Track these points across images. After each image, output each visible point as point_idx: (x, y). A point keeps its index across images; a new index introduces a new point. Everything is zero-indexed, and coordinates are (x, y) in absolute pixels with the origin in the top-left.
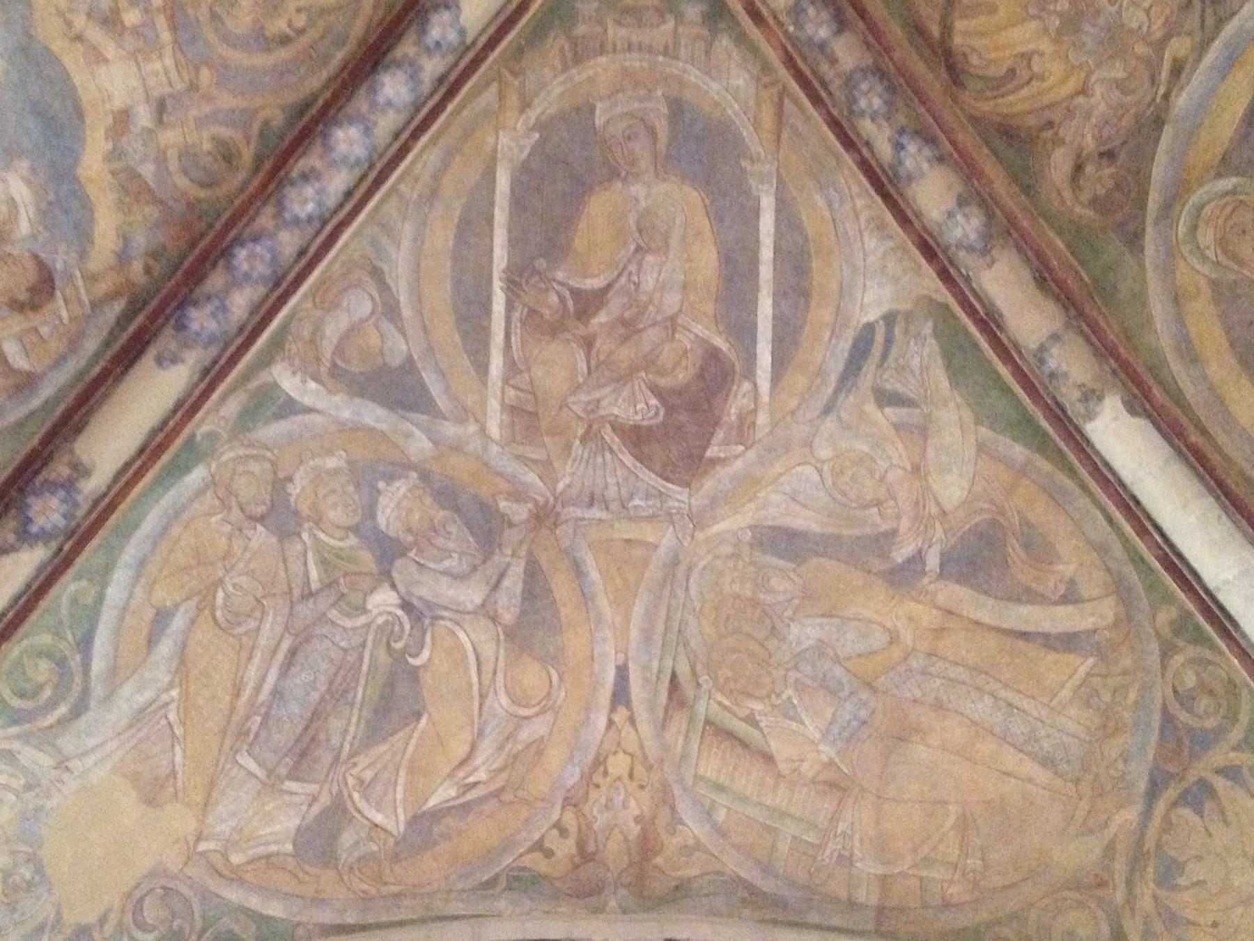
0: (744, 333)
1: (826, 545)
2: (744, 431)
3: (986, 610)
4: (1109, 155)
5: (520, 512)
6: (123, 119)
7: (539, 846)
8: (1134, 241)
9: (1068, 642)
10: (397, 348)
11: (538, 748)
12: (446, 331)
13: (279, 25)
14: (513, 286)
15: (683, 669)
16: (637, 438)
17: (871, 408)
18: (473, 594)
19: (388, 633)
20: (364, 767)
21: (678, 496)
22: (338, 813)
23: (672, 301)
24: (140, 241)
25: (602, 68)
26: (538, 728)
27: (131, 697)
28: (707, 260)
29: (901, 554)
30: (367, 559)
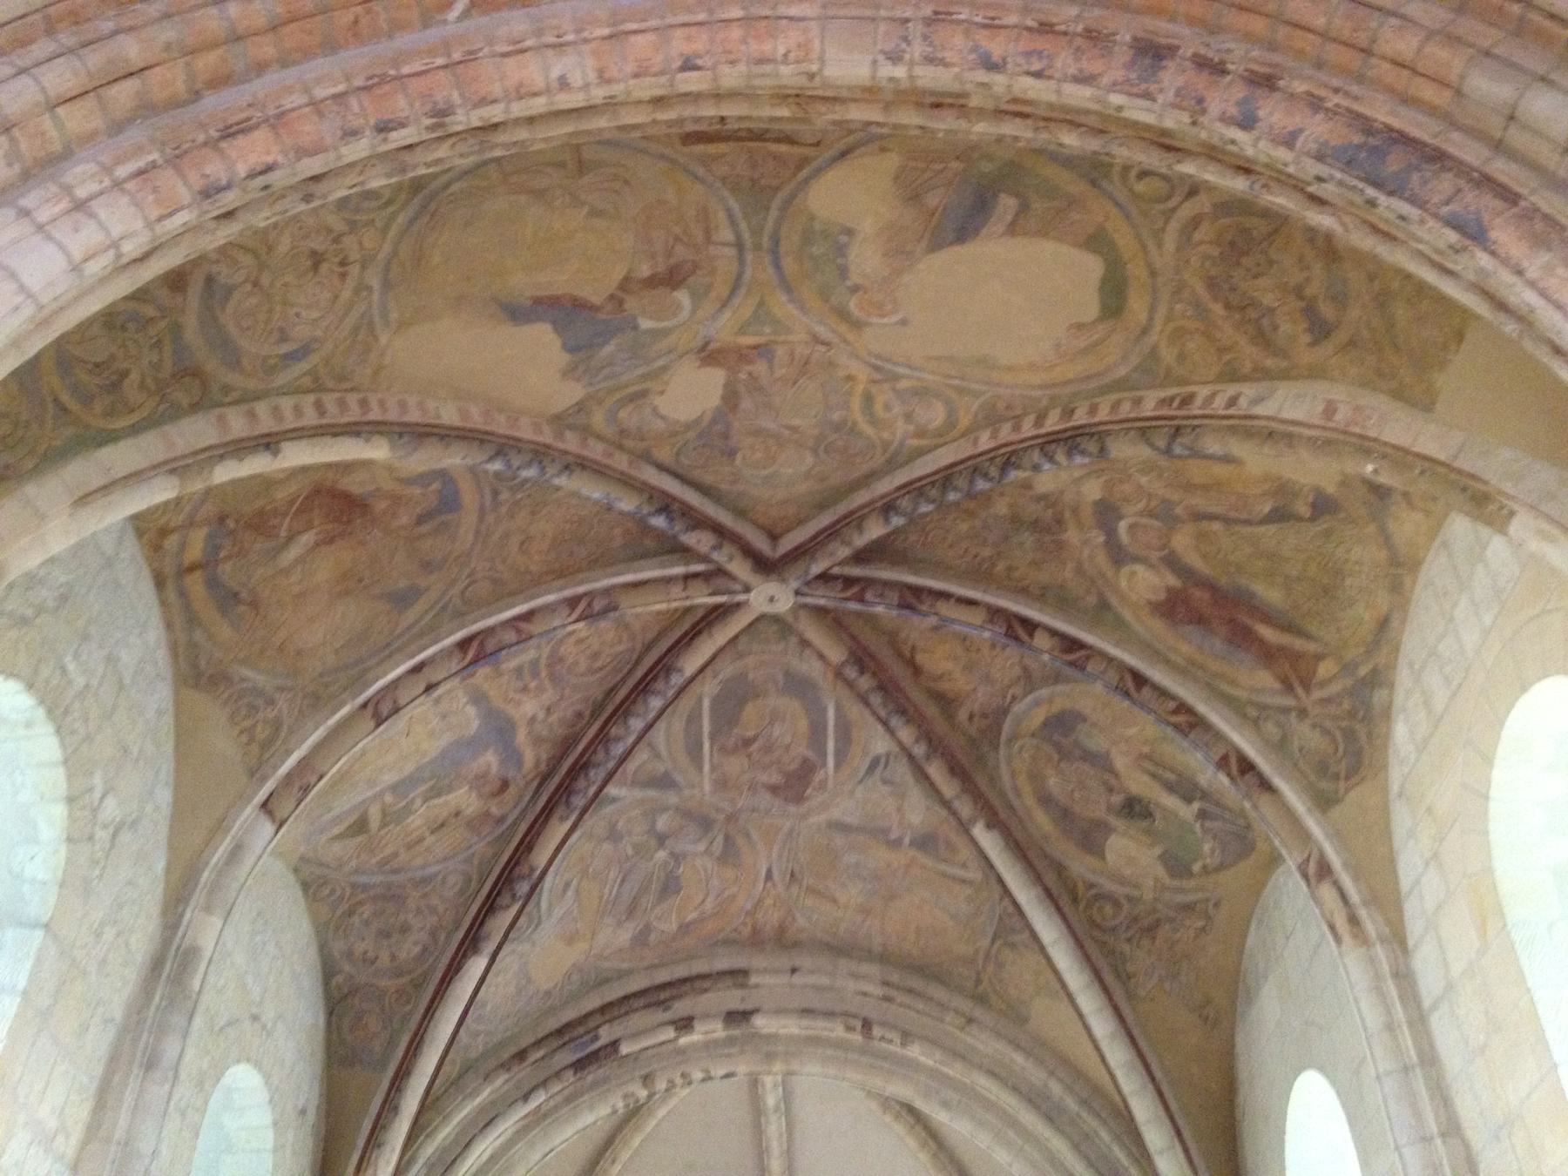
0: (823, 754)
1: (860, 829)
2: (822, 786)
3: (928, 862)
4: (984, 716)
5: (722, 817)
6: (533, 720)
7: (735, 930)
8: (996, 748)
9: (963, 881)
10: (661, 768)
11: (733, 897)
12: (684, 760)
13: (599, 664)
14: (713, 738)
15: (797, 869)
16: (774, 789)
17: (879, 783)
18: (701, 847)
19: (666, 863)
20: (658, 910)
21: (792, 809)
22: (647, 930)
23: (788, 740)
24: (544, 756)
25: (750, 660)
26: (734, 890)
27: (558, 912)
28: (803, 724)
29: (893, 836)
30: (653, 842)
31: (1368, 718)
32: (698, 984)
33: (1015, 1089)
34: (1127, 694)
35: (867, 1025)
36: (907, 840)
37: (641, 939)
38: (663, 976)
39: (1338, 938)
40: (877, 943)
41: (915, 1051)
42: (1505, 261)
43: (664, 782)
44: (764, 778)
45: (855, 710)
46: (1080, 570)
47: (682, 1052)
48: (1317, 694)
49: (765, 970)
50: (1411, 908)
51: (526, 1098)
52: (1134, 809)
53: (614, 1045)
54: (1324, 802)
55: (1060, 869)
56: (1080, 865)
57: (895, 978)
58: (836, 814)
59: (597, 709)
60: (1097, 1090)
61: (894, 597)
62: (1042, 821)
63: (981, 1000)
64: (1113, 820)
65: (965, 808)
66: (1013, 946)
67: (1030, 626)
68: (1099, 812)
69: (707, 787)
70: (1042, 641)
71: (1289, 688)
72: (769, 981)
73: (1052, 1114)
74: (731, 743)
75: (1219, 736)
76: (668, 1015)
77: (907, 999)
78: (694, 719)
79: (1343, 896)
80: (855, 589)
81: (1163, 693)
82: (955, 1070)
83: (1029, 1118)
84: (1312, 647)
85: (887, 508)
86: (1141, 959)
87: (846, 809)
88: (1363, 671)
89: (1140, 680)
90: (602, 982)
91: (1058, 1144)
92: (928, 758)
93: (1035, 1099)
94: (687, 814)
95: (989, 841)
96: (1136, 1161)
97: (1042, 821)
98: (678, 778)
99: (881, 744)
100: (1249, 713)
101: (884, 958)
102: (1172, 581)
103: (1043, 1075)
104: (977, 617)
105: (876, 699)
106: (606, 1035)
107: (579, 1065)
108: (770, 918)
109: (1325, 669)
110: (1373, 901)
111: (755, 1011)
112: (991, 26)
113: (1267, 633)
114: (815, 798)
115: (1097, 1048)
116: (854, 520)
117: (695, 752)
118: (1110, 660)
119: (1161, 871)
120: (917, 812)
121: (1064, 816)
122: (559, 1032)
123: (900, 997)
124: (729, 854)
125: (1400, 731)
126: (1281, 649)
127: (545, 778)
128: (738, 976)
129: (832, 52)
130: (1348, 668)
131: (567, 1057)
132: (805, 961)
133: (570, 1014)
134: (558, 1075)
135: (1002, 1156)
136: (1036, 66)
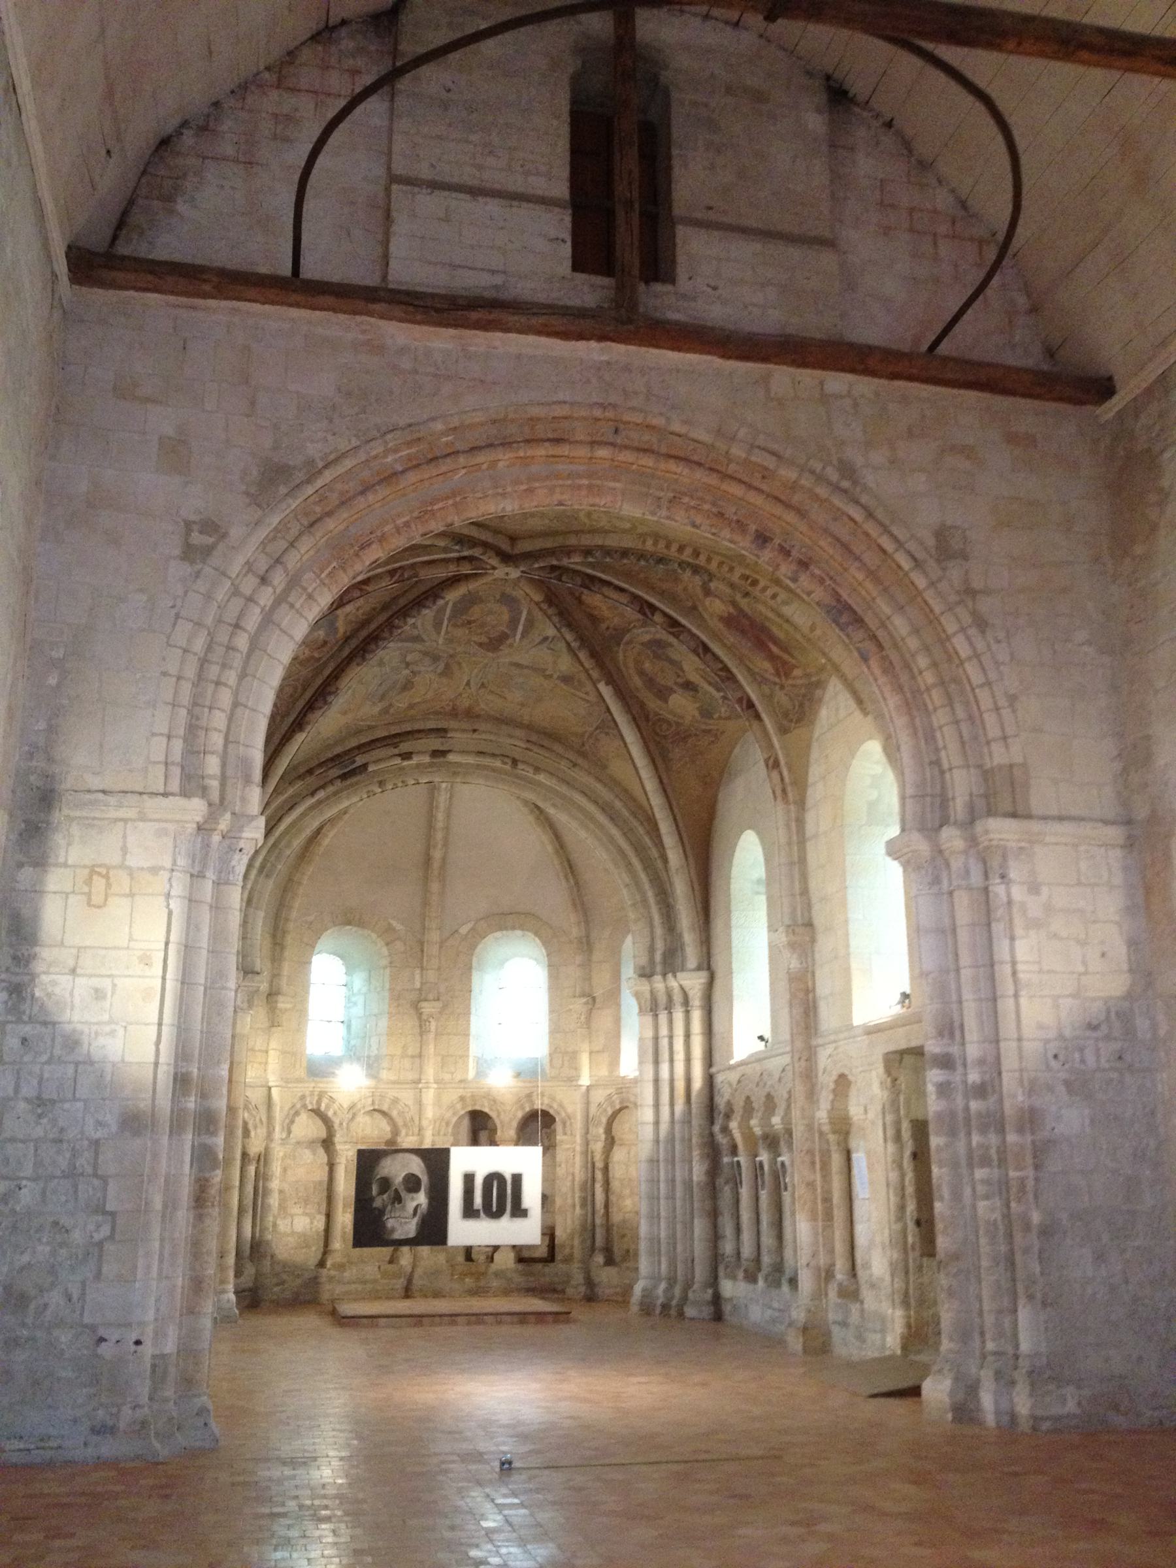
4: (615, 629)
8: (619, 644)
10: (416, 632)
14: (449, 620)
16: (481, 645)
21: (490, 654)
29: (548, 673)
30: (403, 666)
31: (811, 700)
32: (417, 736)
33: (596, 802)
34: (698, 655)
35: (515, 762)
36: (555, 676)
37: (385, 711)
38: (395, 730)
39: (775, 798)
40: (526, 719)
41: (541, 777)
42: (872, 674)
43: (417, 639)
44: (475, 638)
45: (538, 615)
46: (685, 589)
47: (402, 769)
48: (790, 682)
49: (456, 730)
50: (810, 791)
51: (313, 794)
52: (689, 686)
53: (365, 766)
54: (783, 730)
55: (642, 705)
56: (653, 704)
57: (534, 738)
58: (517, 659)
59: (385, 607)
60: (640, 807)
61: (579, 580)
62: (637, 681)
63: (583, 755)
64: (675, 688)
65: (595, 674)
66: (607, 734)
67: (653, 608)
68: (670, 684)
69: (441, 641)
70: (658, 618)
71: (778, 674)
72: (459, 738)
73: (613, 818)
74: (460, 622)
75: (740, 687)
76: (396, 751)
77: (541, 751)
78: (442, 610)
79: (782, 779)
80: (557, 573)
81: (716, 658)
82: (563, 789)
83: (602, 818)
84: (794, 661)
85: (588, 552)
86: (676, 753)
87: (524, 659)
88: (814, 679)
89: (706, 649)
90: (359, 732)
91: (615, 832)
92: (579, 648)
93: (605, 808)
94: (426, 654)
95: (606, 691)
96: (656, 845)
97: (637, 681)
98: (425, 637)
99: (551, 632)
100: (758, 679)
101: (529, 727)
102: (731, 610)
103: (612, 797)
104: (624, 599)
105: (556, 619)
106: (360, 760)
107: (344, 777)
108: (465, 703)
109: (797, 672)
110: (794, 783)
111: (450, 751)
112: (696, 508)
113: (775, 649)
114: (505, 649)
115: (641, 783)
116: (568, 551)
117: (437, 625)
118: (693, 635)
119: (697, 714)
120: (565, 664)
121: (650, 682)
122: (332, 759)
123: (535, 749)
124: (447, 672)
125: (824, 712)
126: (778, 658)
127: (347, 639)
128: (441, 732)
129: (625, 506)
130: (808, 675)
131: (336, 772)
132: (482, 726)
133: (338, 750)
134: (331, 782)
135: (583, 834)
136: (714, 530)
